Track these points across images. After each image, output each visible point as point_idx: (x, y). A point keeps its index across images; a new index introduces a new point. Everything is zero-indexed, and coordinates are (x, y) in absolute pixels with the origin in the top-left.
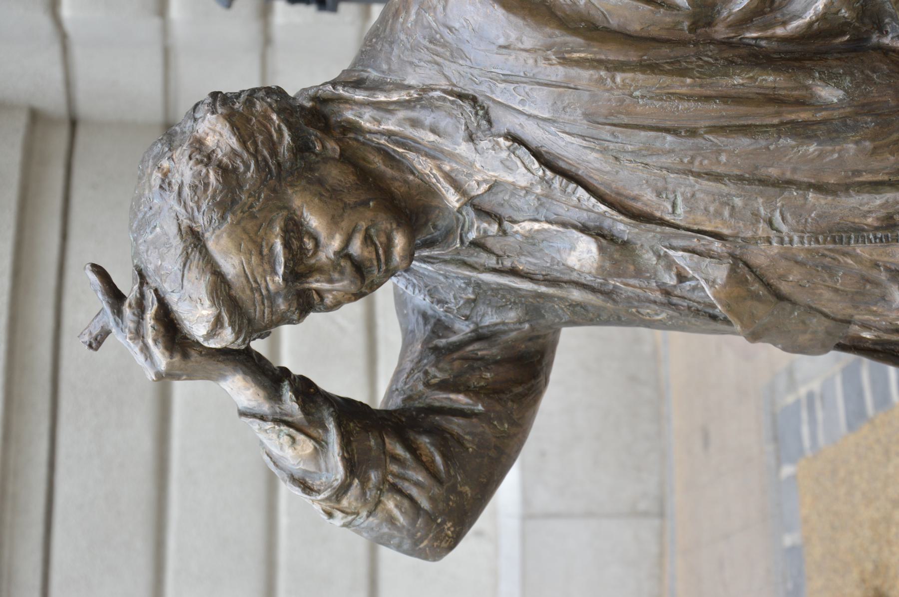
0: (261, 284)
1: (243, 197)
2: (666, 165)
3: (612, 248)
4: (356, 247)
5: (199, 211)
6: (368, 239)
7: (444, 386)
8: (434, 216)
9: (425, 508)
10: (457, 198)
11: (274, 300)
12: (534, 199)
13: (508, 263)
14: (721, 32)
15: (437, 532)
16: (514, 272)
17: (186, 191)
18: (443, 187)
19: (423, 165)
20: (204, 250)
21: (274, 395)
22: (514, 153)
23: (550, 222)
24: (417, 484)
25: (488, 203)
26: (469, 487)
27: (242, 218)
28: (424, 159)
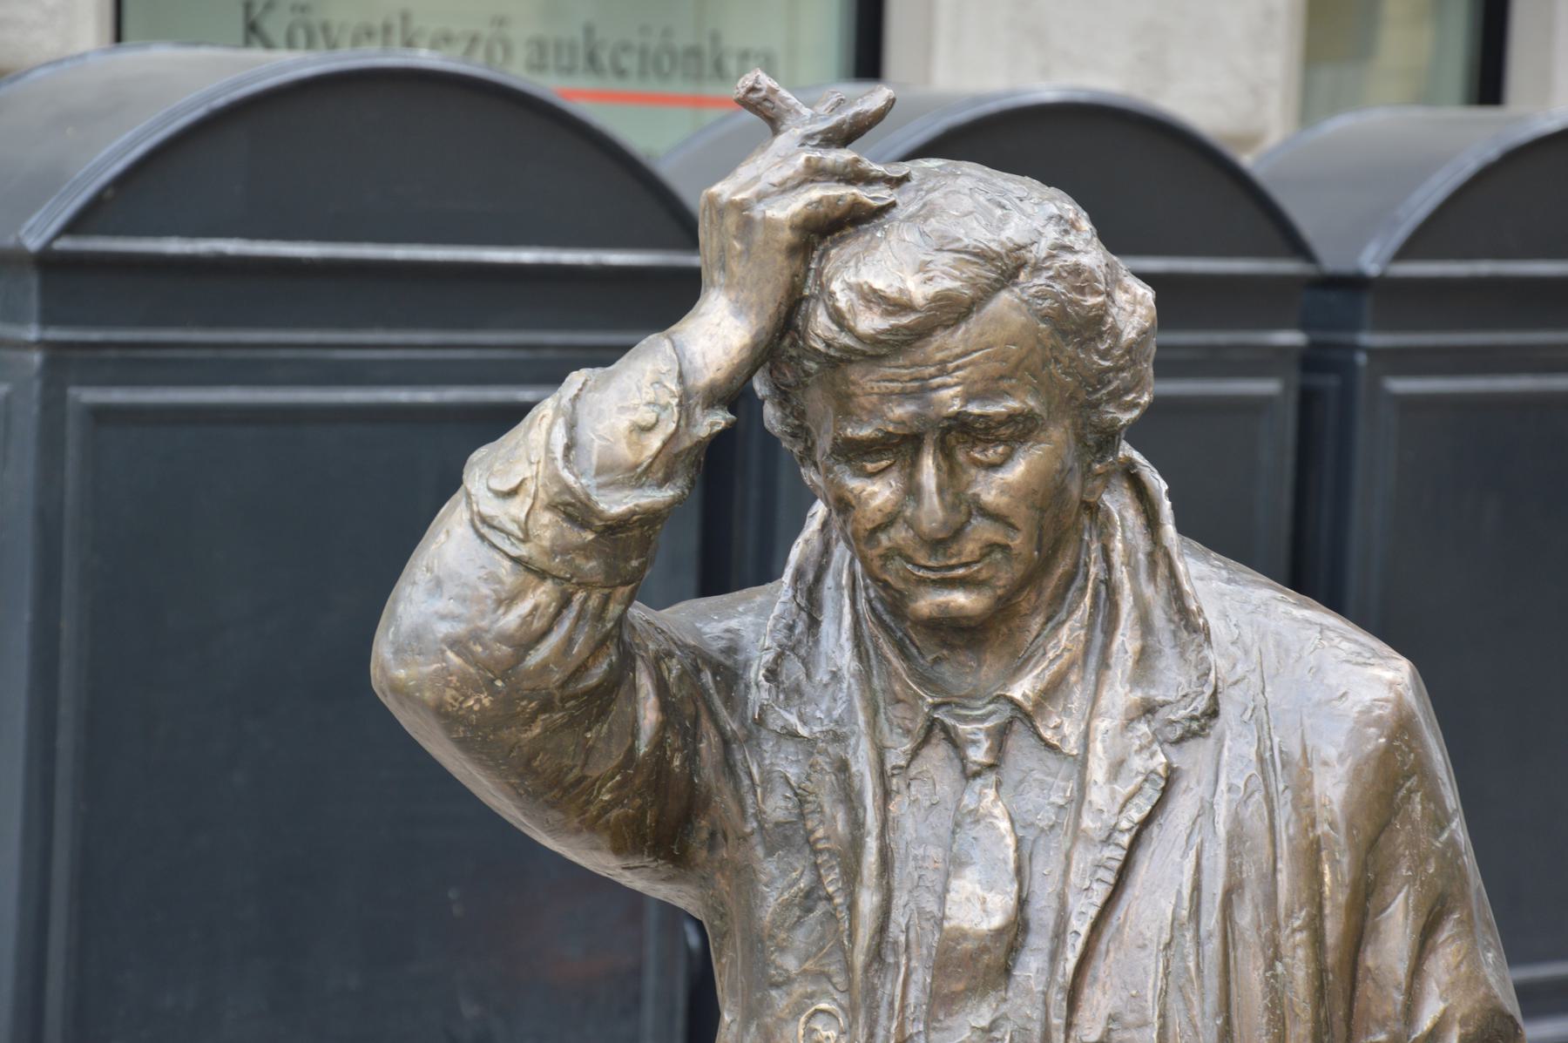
0: (952, 377)
1: (1069, 349)
2: (1170, 1024)
3: (1000, 951)
5: (1050, 278)
7: (661, 687)
8: (962, 658)
9: (528, 658)
10: (1031, 694)
11: (915, 398)
12: (1050, 819)
15: (476, 680)
16: (886, 795)
17: (1070, 259)
18: (1043, 670)
20: (998, 286)
22: (1146, 780)
23: (1018, 849)
24: (569, 641)
25: (1020, 743)
26: (539, 734)
27: (1044, 347)
28: (1082, 638)
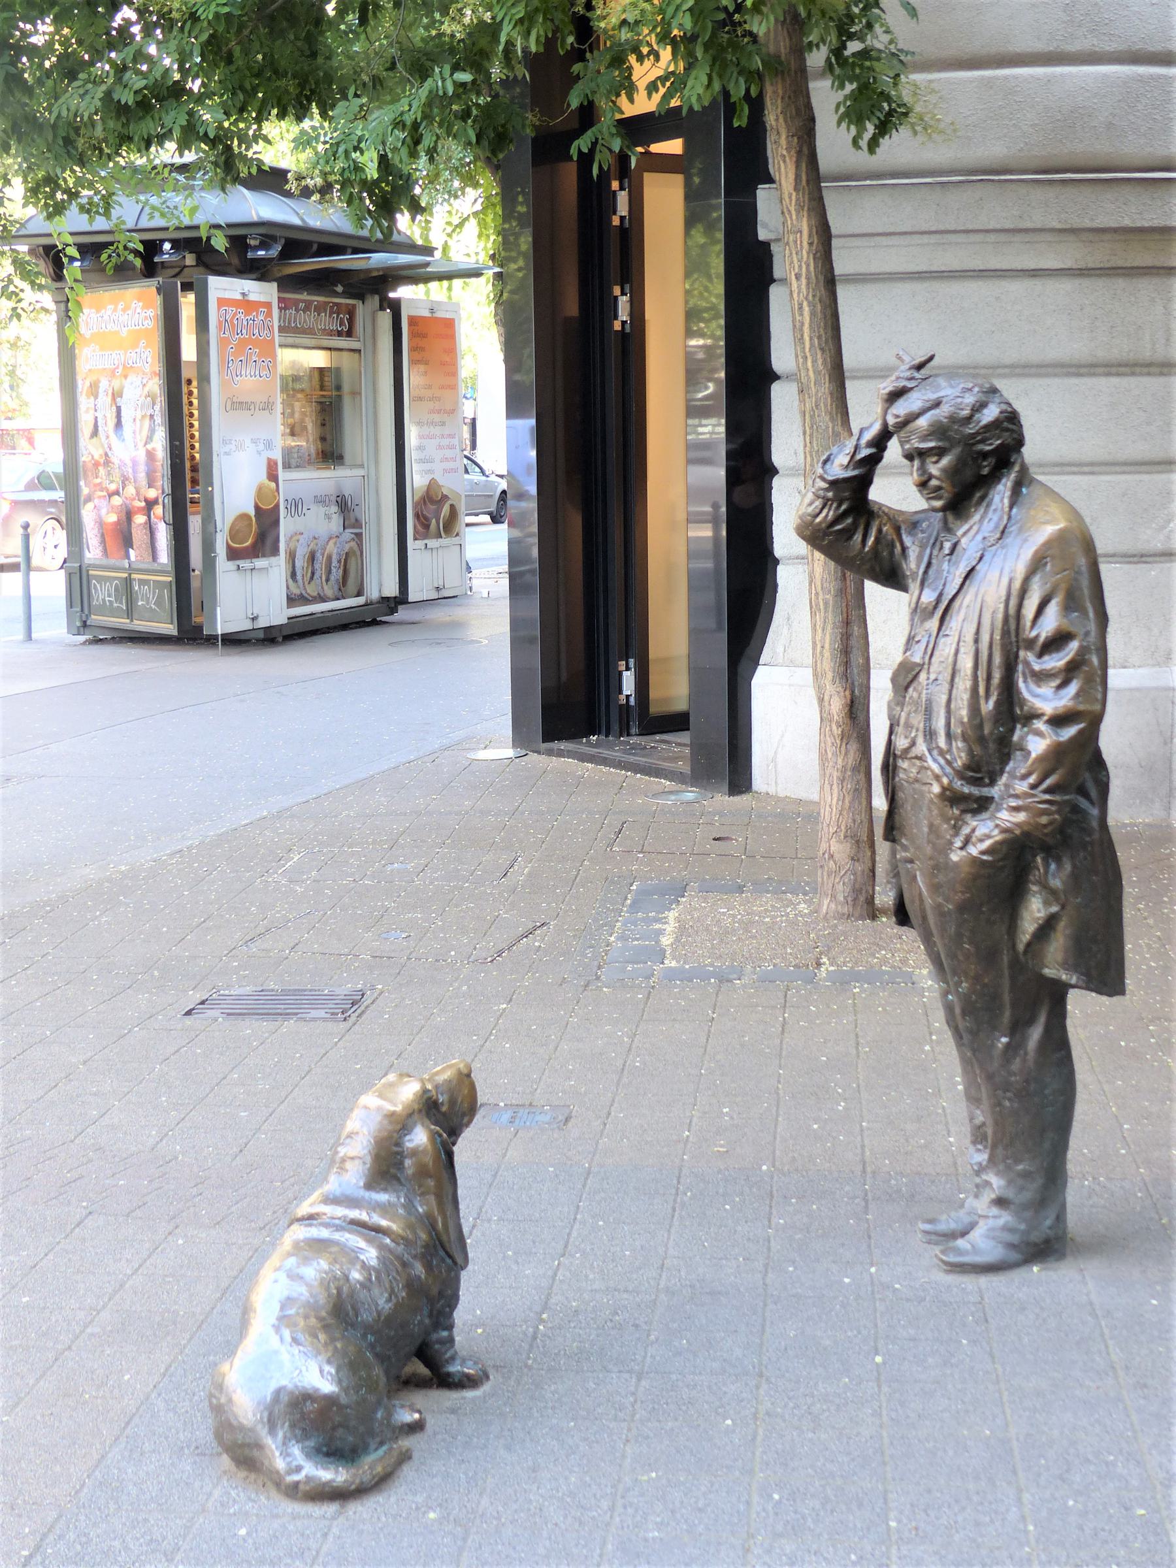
3: (931, 608)
4: (934, 482)
6: (939, 488)
13: (934, 561)
14: (1022, 653)
17: (959, 400)
19: (977, 517)
21: (870, 444)
24: (827, 515)
